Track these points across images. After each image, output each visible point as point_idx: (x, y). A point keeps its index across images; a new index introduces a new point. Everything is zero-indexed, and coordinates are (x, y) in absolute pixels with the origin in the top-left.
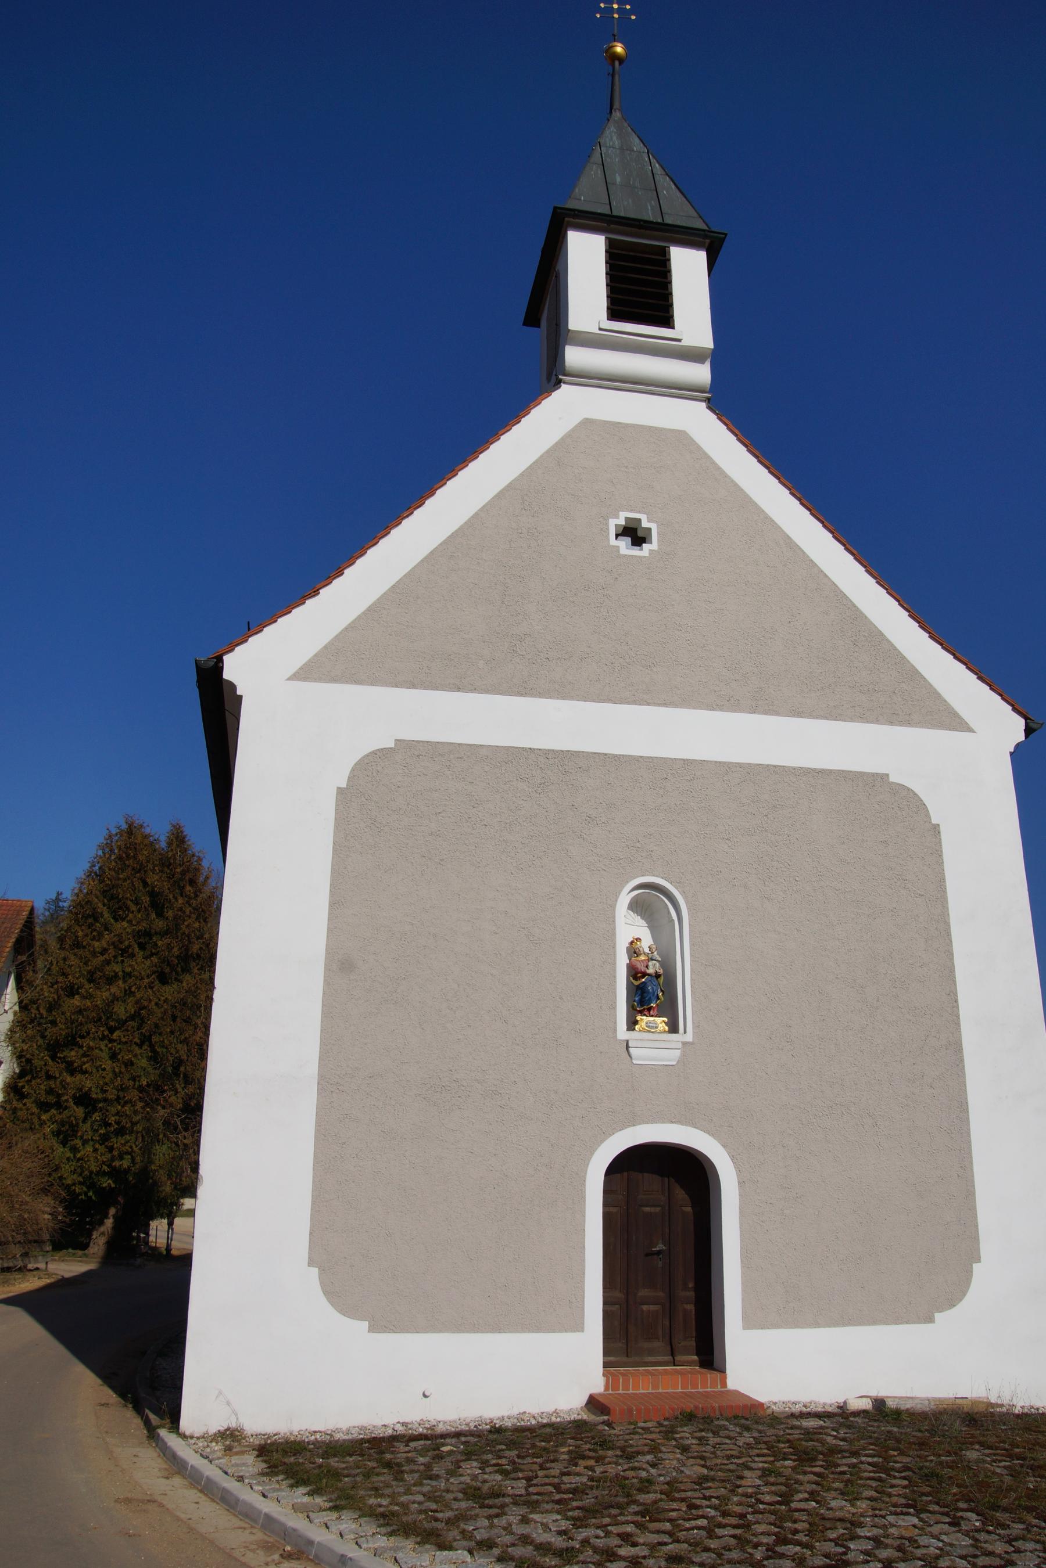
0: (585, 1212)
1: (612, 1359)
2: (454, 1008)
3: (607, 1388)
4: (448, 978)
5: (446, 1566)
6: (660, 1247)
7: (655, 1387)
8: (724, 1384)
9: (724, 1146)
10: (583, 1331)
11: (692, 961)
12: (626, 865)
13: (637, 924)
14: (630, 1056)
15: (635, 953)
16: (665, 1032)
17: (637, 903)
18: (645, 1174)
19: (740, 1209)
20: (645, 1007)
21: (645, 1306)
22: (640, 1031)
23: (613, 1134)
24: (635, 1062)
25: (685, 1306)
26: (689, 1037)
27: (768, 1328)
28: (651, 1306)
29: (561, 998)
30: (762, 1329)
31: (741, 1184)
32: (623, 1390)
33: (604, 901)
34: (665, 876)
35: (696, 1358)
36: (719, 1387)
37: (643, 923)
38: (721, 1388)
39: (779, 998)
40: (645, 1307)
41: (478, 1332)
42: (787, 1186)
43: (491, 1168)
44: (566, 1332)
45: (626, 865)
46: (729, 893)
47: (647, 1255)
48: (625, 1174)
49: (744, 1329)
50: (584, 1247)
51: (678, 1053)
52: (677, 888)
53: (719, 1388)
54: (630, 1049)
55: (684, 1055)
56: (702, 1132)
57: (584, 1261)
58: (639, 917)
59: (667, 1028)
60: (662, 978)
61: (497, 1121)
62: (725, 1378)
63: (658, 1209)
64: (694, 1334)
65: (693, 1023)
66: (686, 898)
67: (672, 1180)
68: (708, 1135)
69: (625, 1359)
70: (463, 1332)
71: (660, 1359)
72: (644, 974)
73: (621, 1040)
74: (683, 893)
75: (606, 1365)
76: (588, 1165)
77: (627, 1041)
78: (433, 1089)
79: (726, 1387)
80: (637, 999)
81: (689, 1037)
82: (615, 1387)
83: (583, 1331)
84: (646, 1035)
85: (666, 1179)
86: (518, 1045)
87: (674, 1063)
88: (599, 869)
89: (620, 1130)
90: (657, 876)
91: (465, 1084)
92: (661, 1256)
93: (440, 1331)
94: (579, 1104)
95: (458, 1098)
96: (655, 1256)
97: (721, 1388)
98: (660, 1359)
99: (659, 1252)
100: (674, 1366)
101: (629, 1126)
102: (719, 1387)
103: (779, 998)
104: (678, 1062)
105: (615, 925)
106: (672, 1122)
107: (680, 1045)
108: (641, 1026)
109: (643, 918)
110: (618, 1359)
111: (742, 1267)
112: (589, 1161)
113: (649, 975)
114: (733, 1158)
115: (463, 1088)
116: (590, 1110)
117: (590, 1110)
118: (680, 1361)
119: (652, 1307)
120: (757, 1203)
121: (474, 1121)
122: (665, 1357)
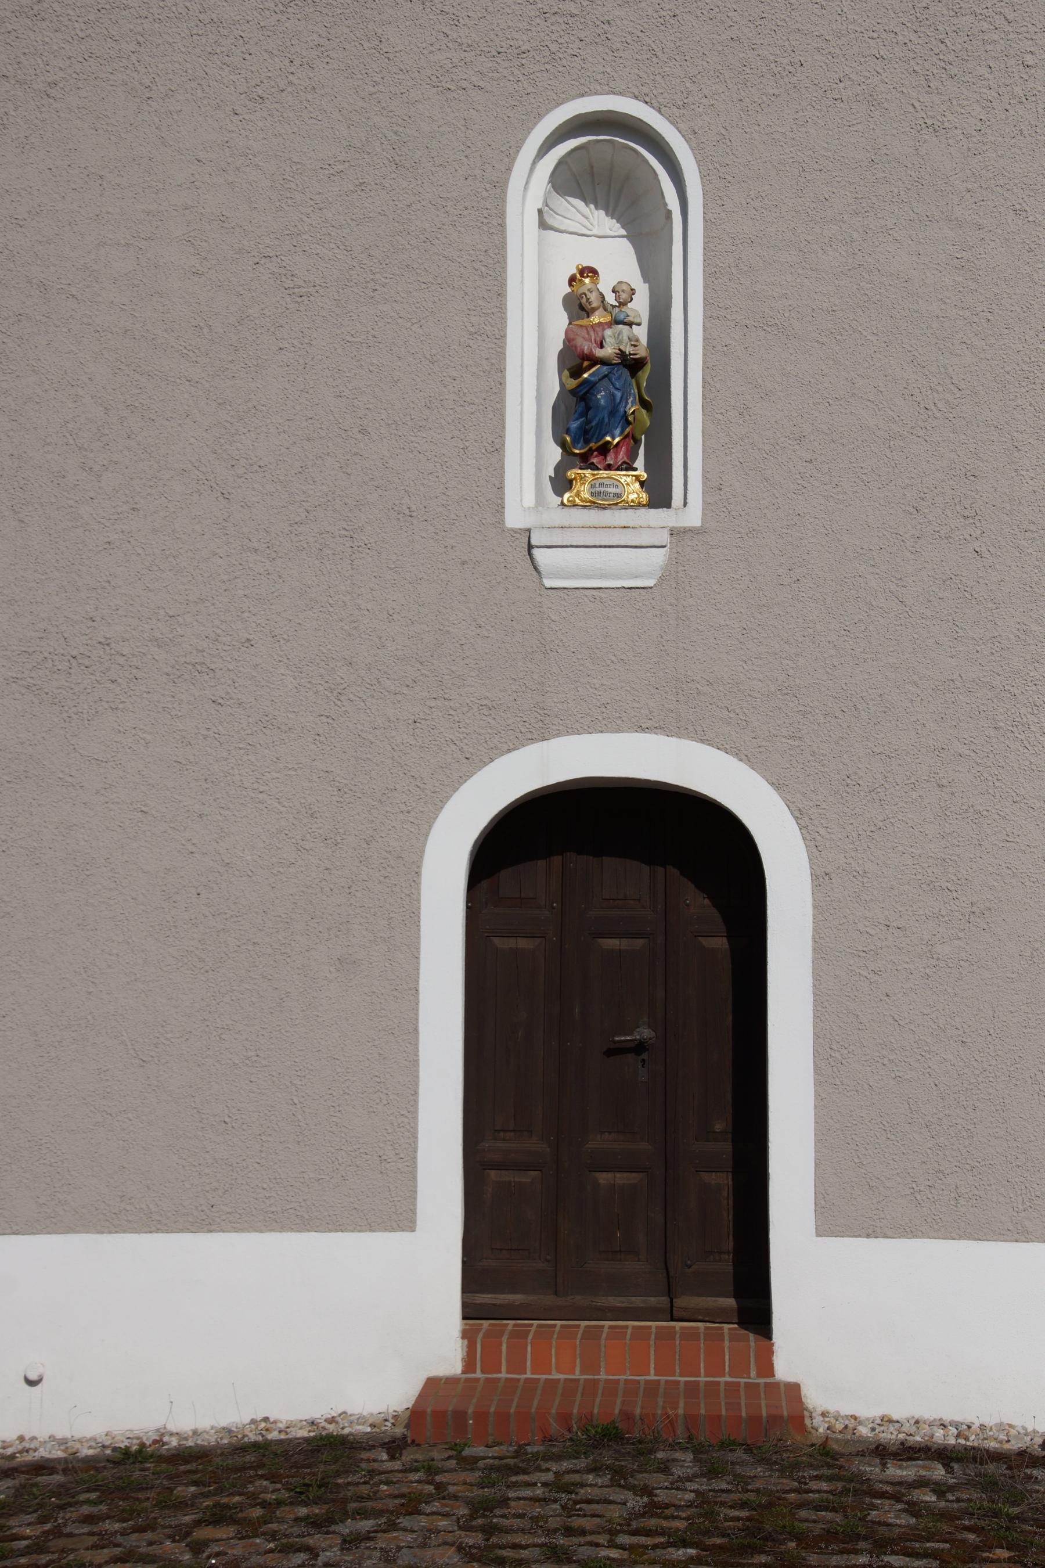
0: (418, 949)
1: (485, 1298)
2: (96, 468)
3: (469, 1364)
4: (81, 392)
5: (977, 1566)
6: (645, 1033)
7: (591, 1366)
8: (767, 1367)
9: (777, 786)
10: (412, 1229)
11: (708, 317)
12: (537, 68)
13: (595, 232)
14: (536, 568)
15: (582, 308)
16: (640, 505)
17: (592, 175)
18: (607, 860)
19: (815, 941)
20: (592, 444)
21: (604, 1175)
22: (575, 505)
23: (492, 760)
24: (548, 583)
25: (706, 1177)
26: (692, 516)
27: (886, 1236)
28: (618, 1175)
29: (363, 431)
30: (868, 1236)
31: (820, 878)
32: (508, 1372)
33: (478, 172)
34: (646, 90)
35: (730, 1302)
36: (753, 1373)
37: (608, 225)
38: (759, 1376)
39: (947, 402)
40: (603, 1178)
41: (158, 1231)
42: (945, 885)
43: (191, 848)
44: (371, 1230)
45: (537, 68)
46: (821, 122)
47: (611, 1052)
48: (557, 860)
49: (818, 1235)
50: (416, 1030)
51: (659, 557)
52: (674, 123)
53: (753, 1377)
54: (536, 552)
55: (676, 561)
56: (722, 754)
57: (416, 1063)
58: (602, 213)
59: (644, 497)
60: (648, 369)
61: (205, 737)
62: (771, 1352)
63: (640, 942)
64: (729, 1244)
65: (705, 478)
66: (697, 149)
67: (674, 871)
68: (735, 760)
69: (548, 1300)
70: (124, 1232)
71: (637, 1301)
72: (595, 361)
73: (515, 531)
74: (691, 136)
75: (467, 1314)
76: (427, 835)
77: (529, 531)
78: (49, 664)
79: (773, 1375)
80: (574, 425)
81: (692, 516)
82: (491, 1364)
83: (412, 1229)
84: (593, 516)
85: (660, 870)
86: (256, 551)
87: (650, 583)
88: (465, 84)
89: (509, 751)
90: (621, 94)
91: (126, 651)
92: (645, 1056)
93: (70, 1229)
94: (405, 690)
95: (109, 685)
96: (630, 1057)
97: (759, 1376)
98: (637, 1301)
99: (640, 1047)
100: (672, 1320)
101: (532, 740)
102: (753, 1373)
103: (947, 402)
104: (662, 579)
105: (504, 237)
106: (642, 729)
107: (664, 538)
108: (578, 495)
109: (611, 212)
110: (531, 1298)
111: (818, 1083)
112: (430, 827)
113: (603, 362)
114: (799, 815)
115: (121, 660)
116: (433, 703)
117: (433, 703)
118: (685, 1309)
119: (621, 1178)
120: (861, 927)
121: (149, 737)
122: (652, 1299)
